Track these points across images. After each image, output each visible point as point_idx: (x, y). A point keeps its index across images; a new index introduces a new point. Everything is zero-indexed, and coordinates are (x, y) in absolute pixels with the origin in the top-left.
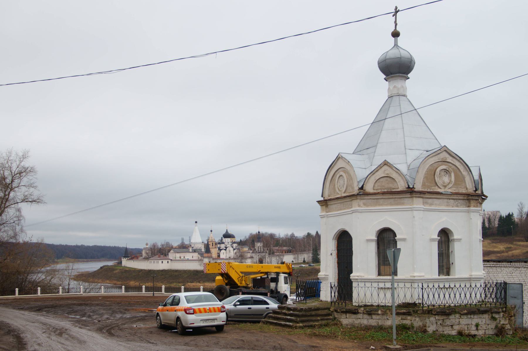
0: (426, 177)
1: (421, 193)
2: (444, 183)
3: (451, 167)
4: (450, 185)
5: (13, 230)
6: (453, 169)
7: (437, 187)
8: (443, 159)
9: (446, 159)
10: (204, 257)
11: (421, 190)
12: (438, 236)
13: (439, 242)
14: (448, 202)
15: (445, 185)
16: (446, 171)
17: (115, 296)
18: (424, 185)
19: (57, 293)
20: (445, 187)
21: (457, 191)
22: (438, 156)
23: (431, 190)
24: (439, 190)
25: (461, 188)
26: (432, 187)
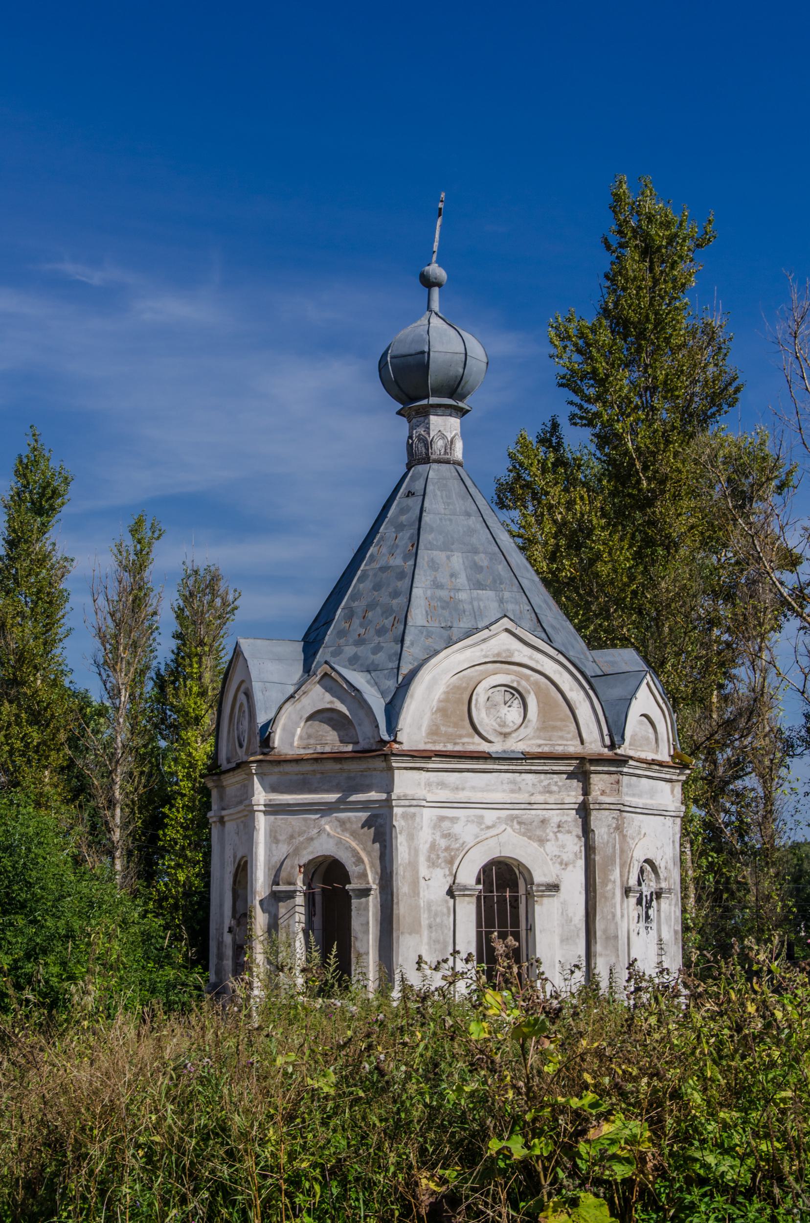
0: (443, 711)
1: (426, 756)
2: (503, 724)
3: (527, 678)
4: (523, 732)
5: (727, 1056)
6: (536, 683)
7: (477, 739)
8: (498, 655)
9: (512, 655)
10: (767, 873)
11: (422, 747)
12: (478, 882)
13: (479, 898)
14: (514, 782)
15: (507, 730)
16: (516, 693)
17: (289, 805)
18: (434, 732)
19: (442, 819)
20: (506, 735)
21: (546, 749)
22: (484, 646)
23: (458, 748)
24: (485, 747)
25: (562, 738)
26: (461, 737)
